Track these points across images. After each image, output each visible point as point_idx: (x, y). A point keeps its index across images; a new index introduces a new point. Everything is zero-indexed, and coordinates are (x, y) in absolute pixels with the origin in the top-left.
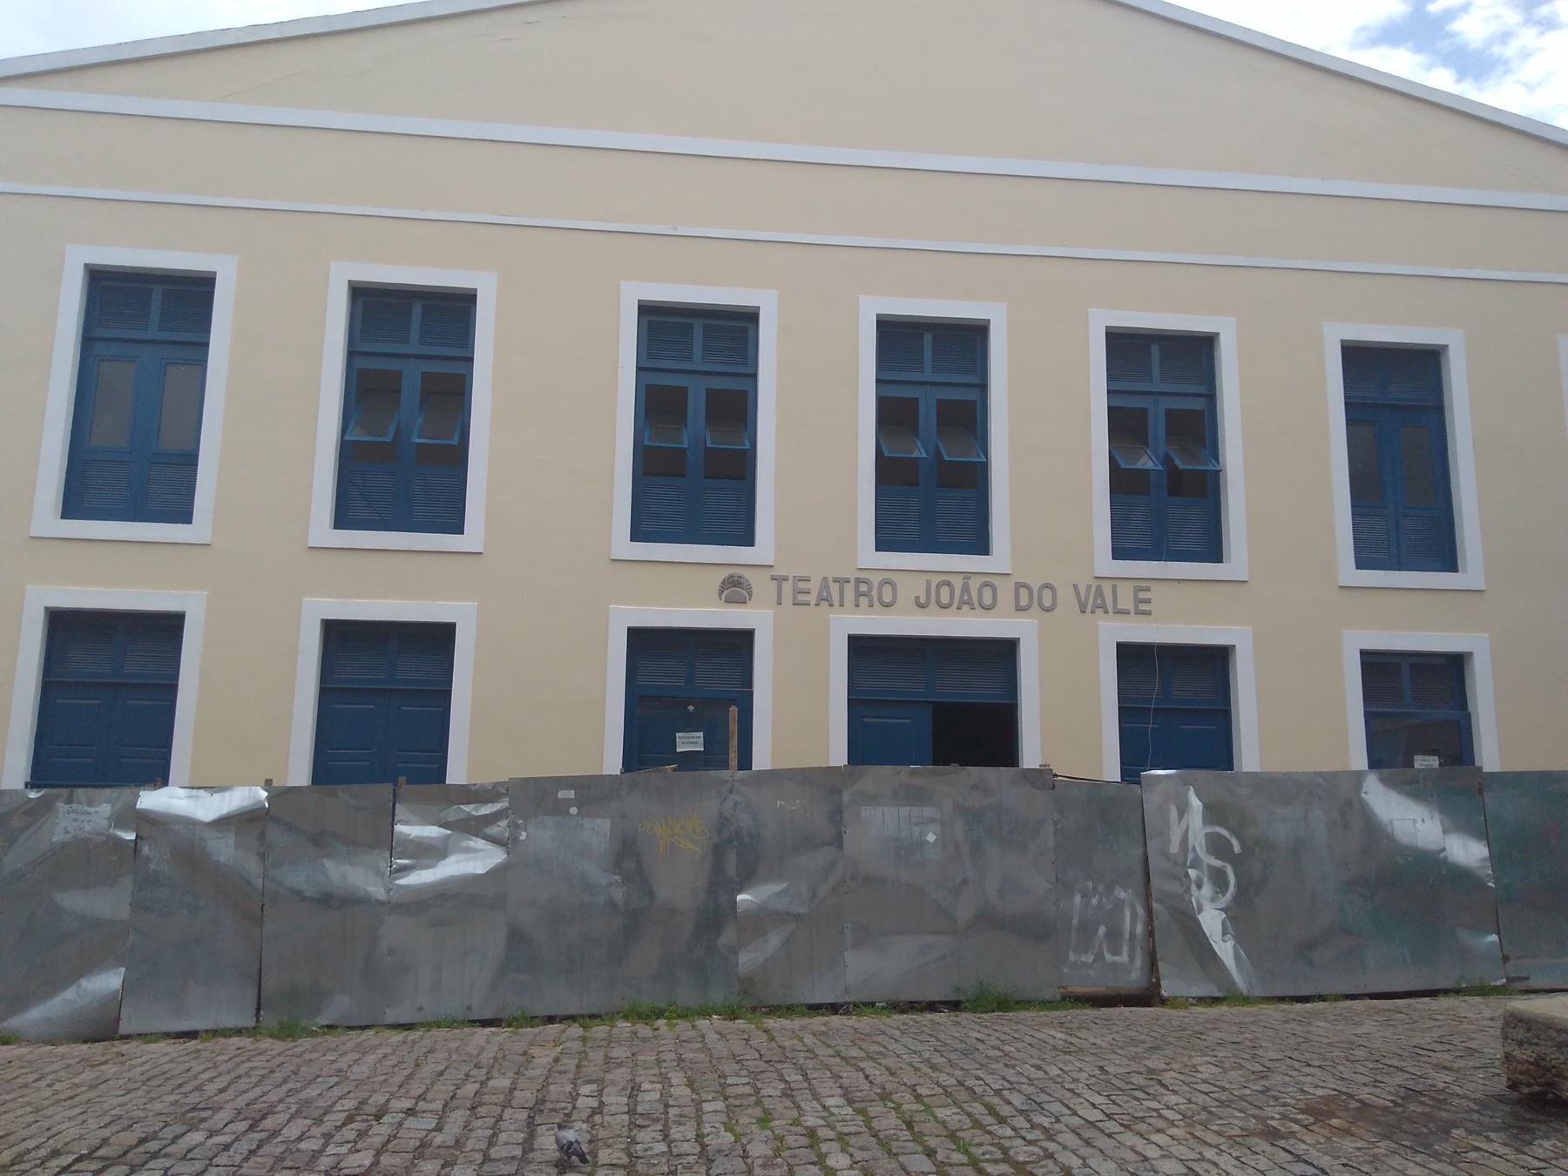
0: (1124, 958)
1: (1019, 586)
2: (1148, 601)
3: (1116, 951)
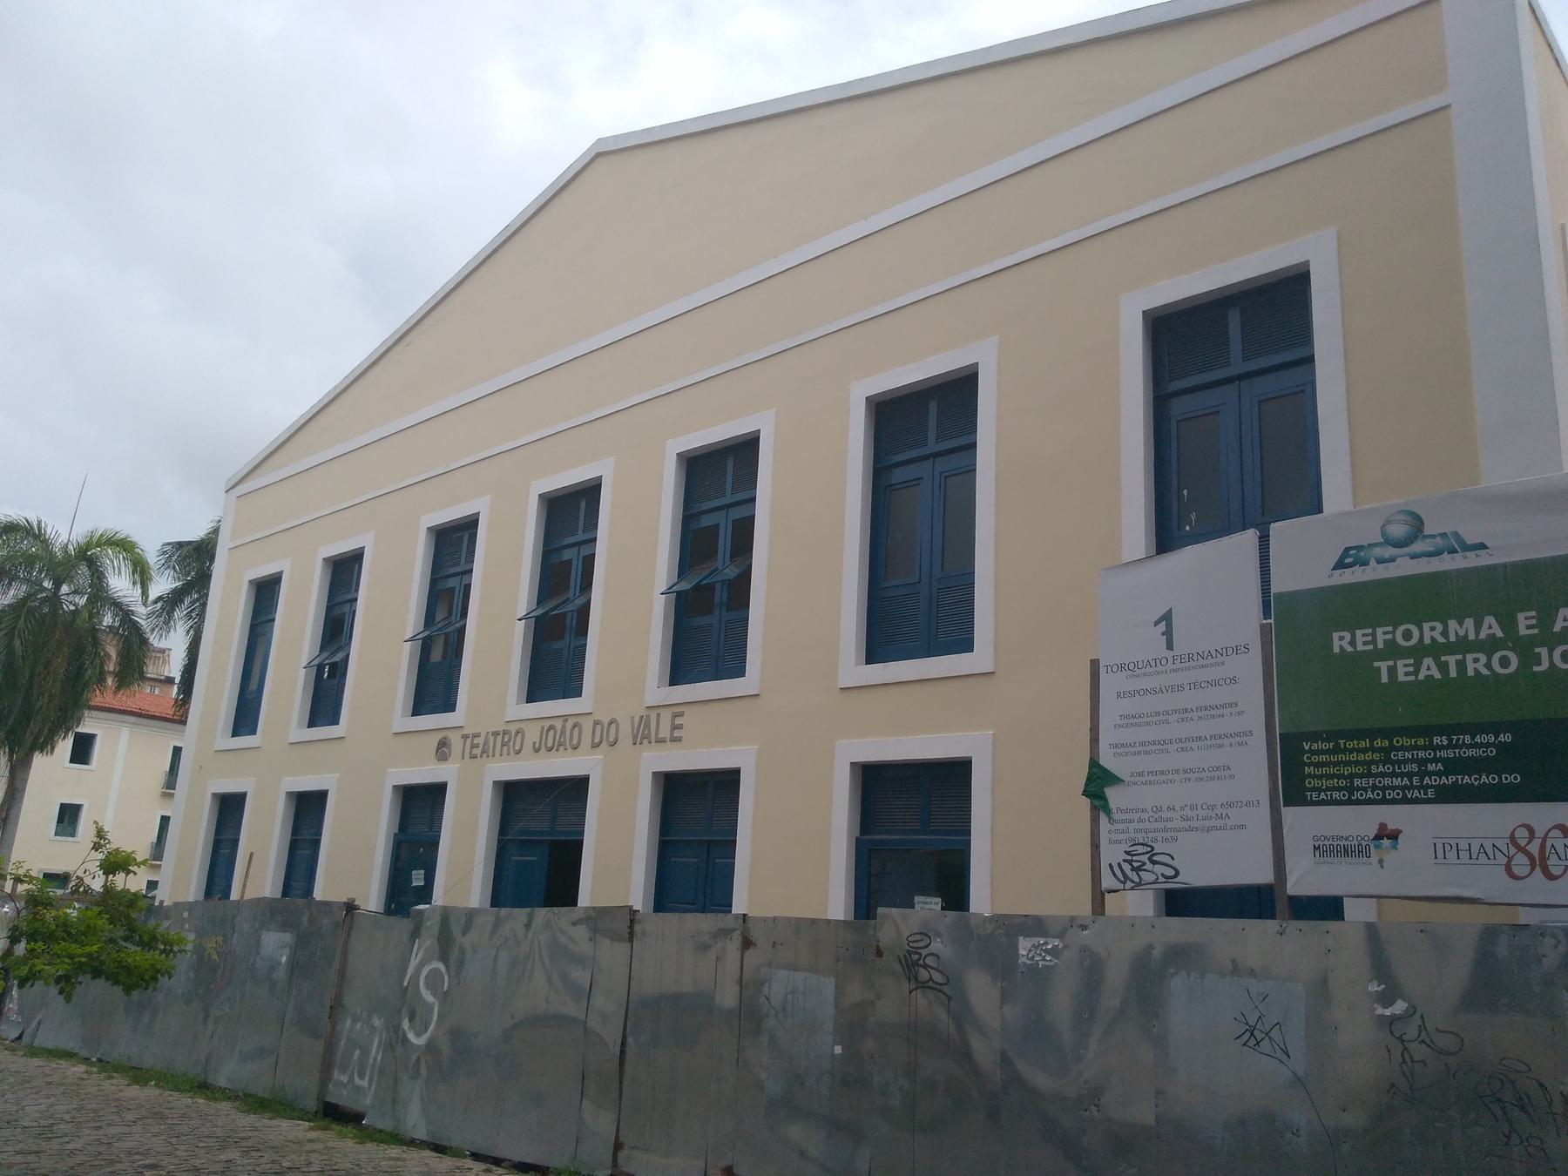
0: (364, 1083)
1: (596, 723)
2: (680, 727)
3: (362, 1077)
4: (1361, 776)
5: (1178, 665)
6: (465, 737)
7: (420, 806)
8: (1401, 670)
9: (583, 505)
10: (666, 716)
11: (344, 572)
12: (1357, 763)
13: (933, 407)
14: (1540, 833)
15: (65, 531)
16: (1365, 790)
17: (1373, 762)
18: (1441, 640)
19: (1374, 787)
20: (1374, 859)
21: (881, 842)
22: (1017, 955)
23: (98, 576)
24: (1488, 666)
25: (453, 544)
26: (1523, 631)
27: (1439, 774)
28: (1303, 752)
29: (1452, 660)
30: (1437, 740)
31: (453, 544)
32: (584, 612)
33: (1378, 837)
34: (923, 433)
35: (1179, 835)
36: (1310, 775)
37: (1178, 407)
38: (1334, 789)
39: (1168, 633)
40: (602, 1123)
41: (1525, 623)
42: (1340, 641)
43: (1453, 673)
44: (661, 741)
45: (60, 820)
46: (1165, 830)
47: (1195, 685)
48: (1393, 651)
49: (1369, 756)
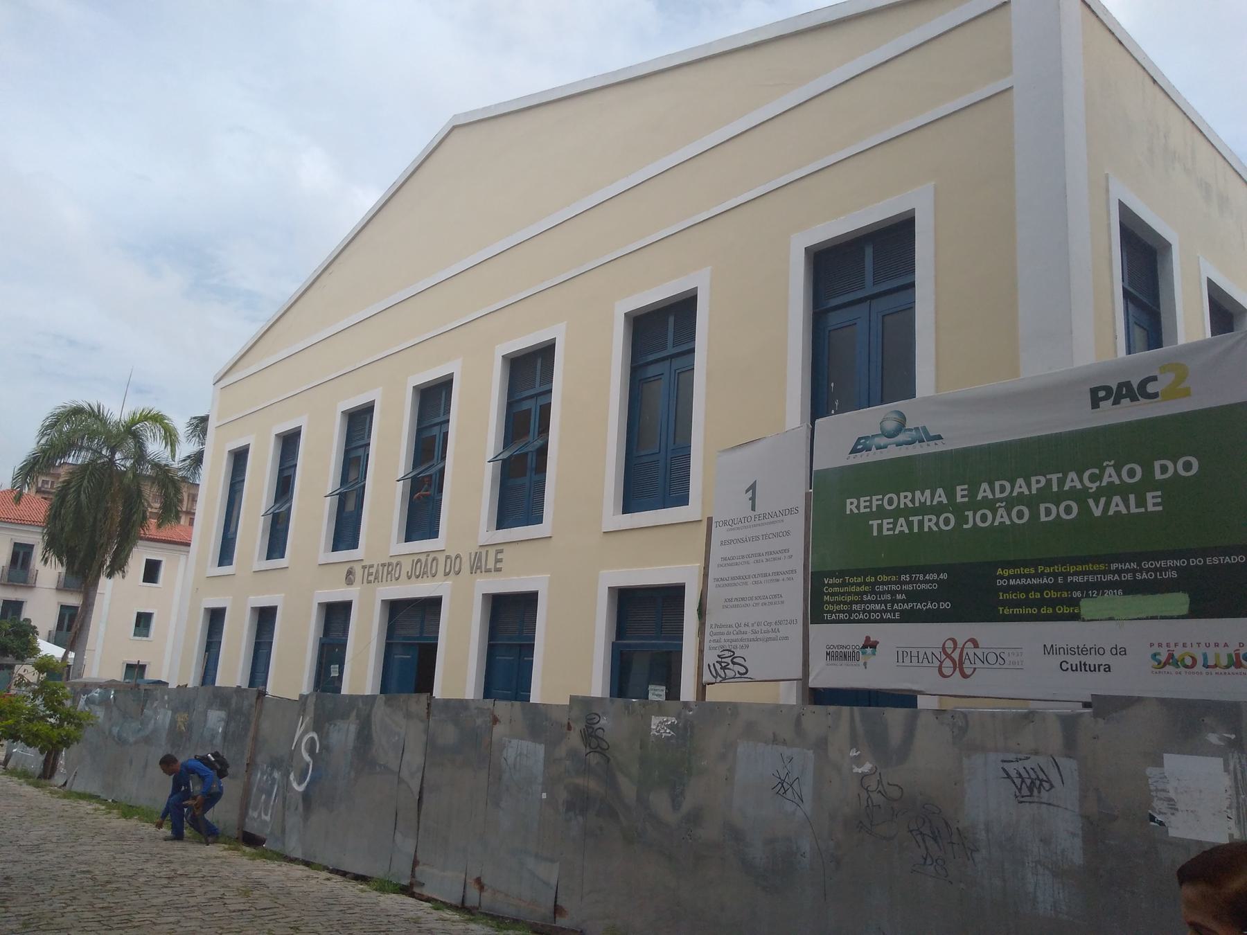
0: (268, 818)
1: (448, 557)
4: (857, 603)
5: (757, 522)
6: (364, 567)
7: (336, 616)
8: (885, 527)
9: (539, 361)
10: (492, 552)
11: (289, 442)
12: (856, 593)
13: (869, 252)
14: (960, 645)
15: (117, 411)
16: (858, 612)
17: (865, 593)
18: (910, 505)
19: (864, 611)
20: (861, 662)
21: (629, 646)
22: (650, 729)
23: (140, 446)
24: (937, 524)
25: (358, 422)
26: (959, 500)
27: (903, 601)
28: (824, 585)
29: (915, 519)
30: (903, 578)
31: (358, 422)
32: (543, 452)
33: (865, 647)
34: (661, 336)
35: (751, 644)
36: (827, 602)
37: (834, 319)
38: (840, 612)
39: (753, 499)
40: (407, 845)
41: (960, 492)
42: (851, 506)
43: (916, 530)
44: (488, 571)
45: (137, 625)
46: (742, 640)
47: (766, 537)
48: (881, 513)
49: (863, 588)
